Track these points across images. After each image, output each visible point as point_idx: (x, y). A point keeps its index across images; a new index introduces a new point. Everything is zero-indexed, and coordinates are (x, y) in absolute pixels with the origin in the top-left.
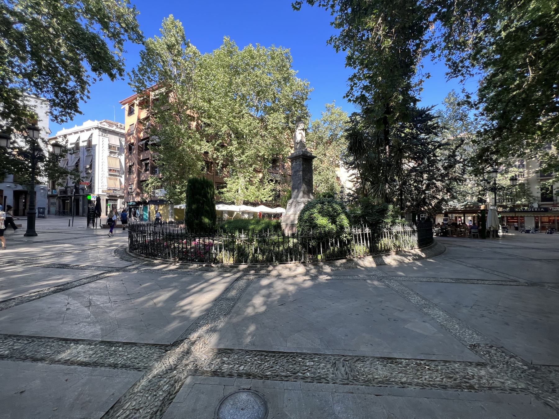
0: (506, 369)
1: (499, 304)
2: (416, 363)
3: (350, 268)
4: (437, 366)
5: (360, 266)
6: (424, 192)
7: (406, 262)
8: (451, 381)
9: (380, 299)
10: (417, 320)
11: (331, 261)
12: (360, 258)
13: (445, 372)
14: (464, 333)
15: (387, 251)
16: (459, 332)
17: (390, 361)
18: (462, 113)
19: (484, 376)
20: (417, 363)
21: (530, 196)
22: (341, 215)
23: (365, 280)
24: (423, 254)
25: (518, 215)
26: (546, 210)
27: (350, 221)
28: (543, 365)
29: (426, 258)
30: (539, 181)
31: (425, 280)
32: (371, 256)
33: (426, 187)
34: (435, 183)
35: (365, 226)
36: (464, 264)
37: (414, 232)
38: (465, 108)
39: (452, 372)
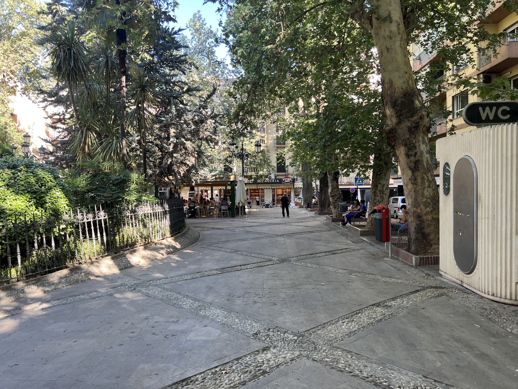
0: (283, 345)
1: (264, 287)
2: (212, 373)
3: (77, 281)
4: (232, 367)
5: (94, 275)
6: (171, 154)
7: (159, 258)
8: (247, 375)
9: (143, 315)
10: (197, 328)
11: (39, 277)
12: (92, 263)
13: (241, 369)
14: (245, 325)
15: (131, 246)
16: (240, 326)
17: (184, 383)
18: (209, 48)
19: (271, 358)
20: (212, 372)
21: (270, 166)
22: (54, 191)
23: (111, 295)
24: (177, 243)
25: (260, 187)
26: (281, 182)
27: (70, 201)
28: (306, 331)
29: (182, 249)
30: (276, 148)
31: (189, 277)
32: (109, 257)
33: (173, 148)
34: (185, 144)
35: (98, 209)
36: (223, 249)
37: (165, 213)
38: (212, 42)
39: (246, 366)
